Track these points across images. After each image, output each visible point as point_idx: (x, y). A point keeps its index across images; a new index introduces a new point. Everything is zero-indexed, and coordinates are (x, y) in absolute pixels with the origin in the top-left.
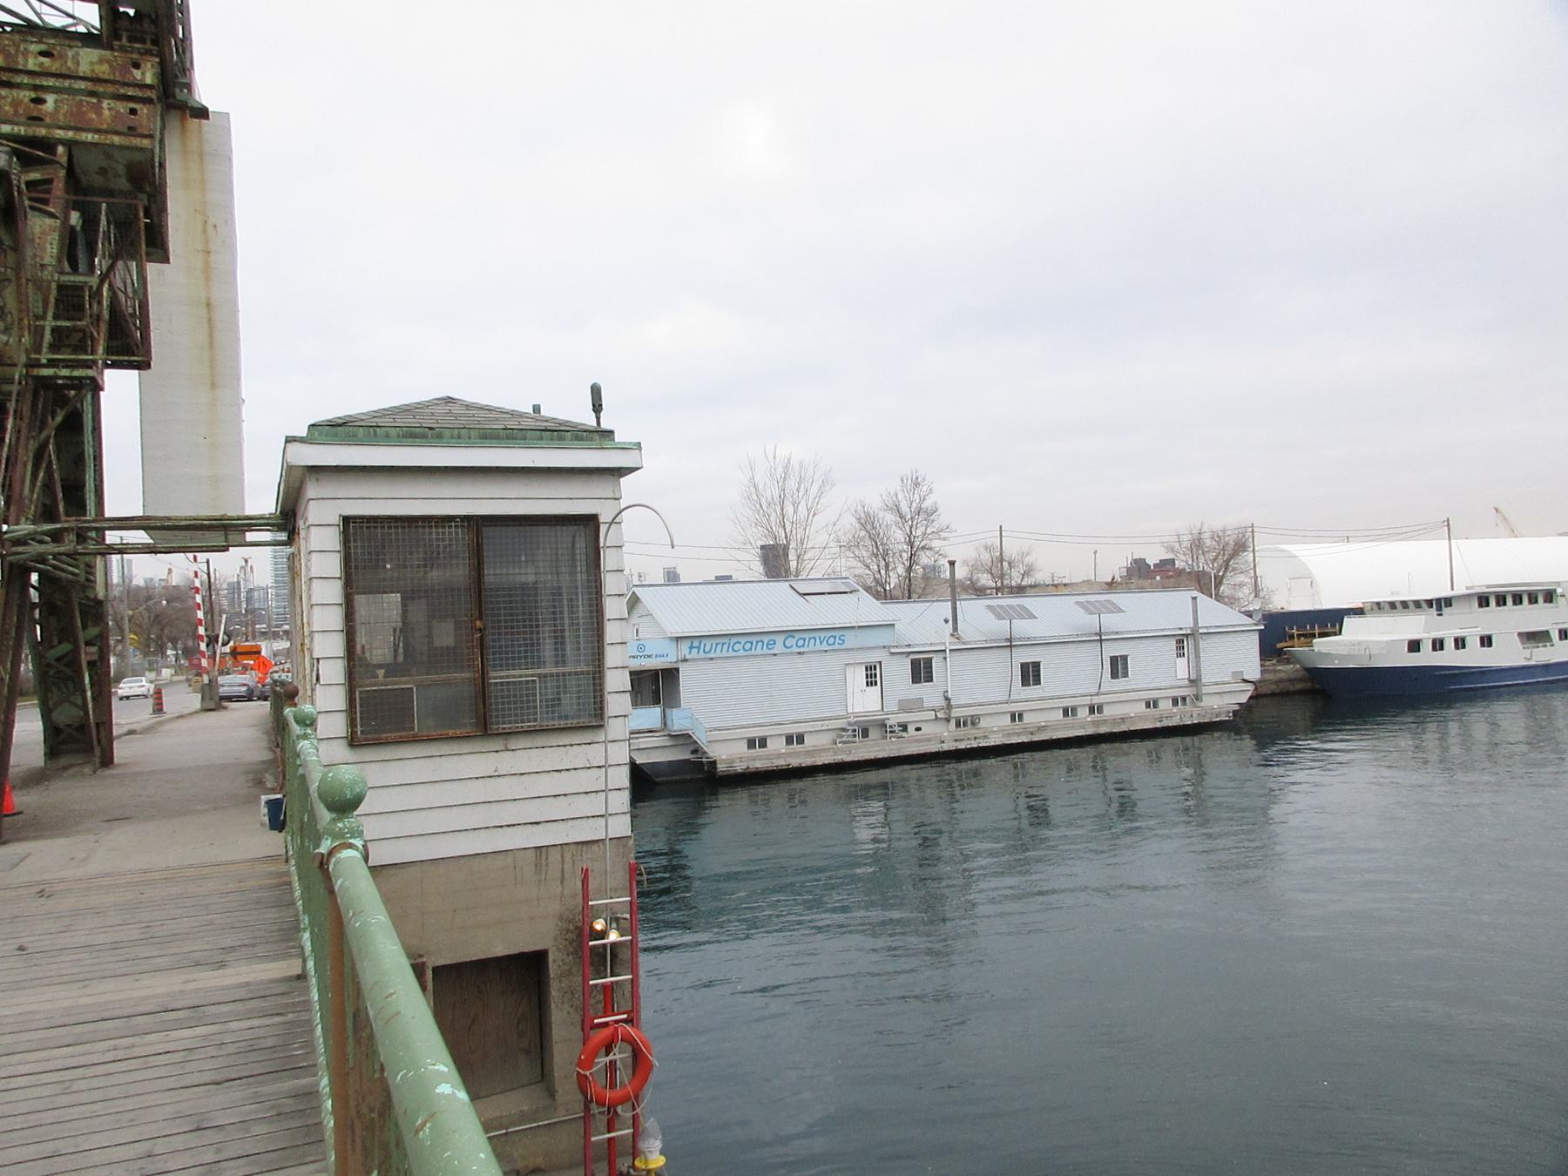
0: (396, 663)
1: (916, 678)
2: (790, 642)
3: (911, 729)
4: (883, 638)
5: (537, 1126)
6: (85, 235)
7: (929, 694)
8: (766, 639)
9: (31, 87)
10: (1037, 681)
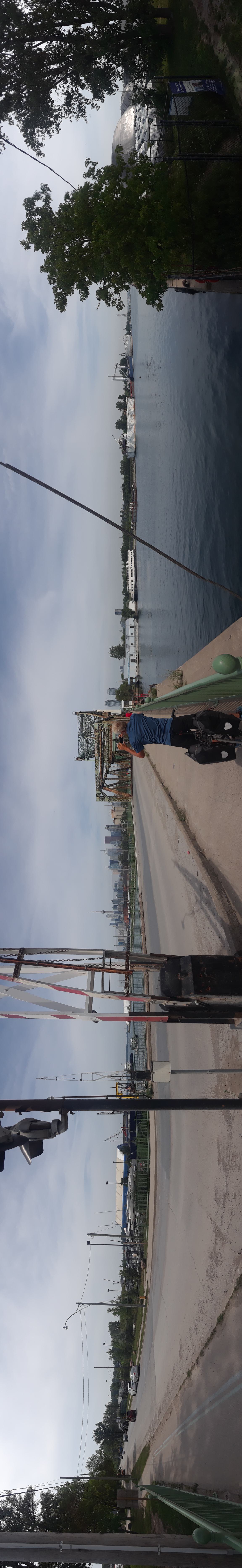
7: (134, 654)
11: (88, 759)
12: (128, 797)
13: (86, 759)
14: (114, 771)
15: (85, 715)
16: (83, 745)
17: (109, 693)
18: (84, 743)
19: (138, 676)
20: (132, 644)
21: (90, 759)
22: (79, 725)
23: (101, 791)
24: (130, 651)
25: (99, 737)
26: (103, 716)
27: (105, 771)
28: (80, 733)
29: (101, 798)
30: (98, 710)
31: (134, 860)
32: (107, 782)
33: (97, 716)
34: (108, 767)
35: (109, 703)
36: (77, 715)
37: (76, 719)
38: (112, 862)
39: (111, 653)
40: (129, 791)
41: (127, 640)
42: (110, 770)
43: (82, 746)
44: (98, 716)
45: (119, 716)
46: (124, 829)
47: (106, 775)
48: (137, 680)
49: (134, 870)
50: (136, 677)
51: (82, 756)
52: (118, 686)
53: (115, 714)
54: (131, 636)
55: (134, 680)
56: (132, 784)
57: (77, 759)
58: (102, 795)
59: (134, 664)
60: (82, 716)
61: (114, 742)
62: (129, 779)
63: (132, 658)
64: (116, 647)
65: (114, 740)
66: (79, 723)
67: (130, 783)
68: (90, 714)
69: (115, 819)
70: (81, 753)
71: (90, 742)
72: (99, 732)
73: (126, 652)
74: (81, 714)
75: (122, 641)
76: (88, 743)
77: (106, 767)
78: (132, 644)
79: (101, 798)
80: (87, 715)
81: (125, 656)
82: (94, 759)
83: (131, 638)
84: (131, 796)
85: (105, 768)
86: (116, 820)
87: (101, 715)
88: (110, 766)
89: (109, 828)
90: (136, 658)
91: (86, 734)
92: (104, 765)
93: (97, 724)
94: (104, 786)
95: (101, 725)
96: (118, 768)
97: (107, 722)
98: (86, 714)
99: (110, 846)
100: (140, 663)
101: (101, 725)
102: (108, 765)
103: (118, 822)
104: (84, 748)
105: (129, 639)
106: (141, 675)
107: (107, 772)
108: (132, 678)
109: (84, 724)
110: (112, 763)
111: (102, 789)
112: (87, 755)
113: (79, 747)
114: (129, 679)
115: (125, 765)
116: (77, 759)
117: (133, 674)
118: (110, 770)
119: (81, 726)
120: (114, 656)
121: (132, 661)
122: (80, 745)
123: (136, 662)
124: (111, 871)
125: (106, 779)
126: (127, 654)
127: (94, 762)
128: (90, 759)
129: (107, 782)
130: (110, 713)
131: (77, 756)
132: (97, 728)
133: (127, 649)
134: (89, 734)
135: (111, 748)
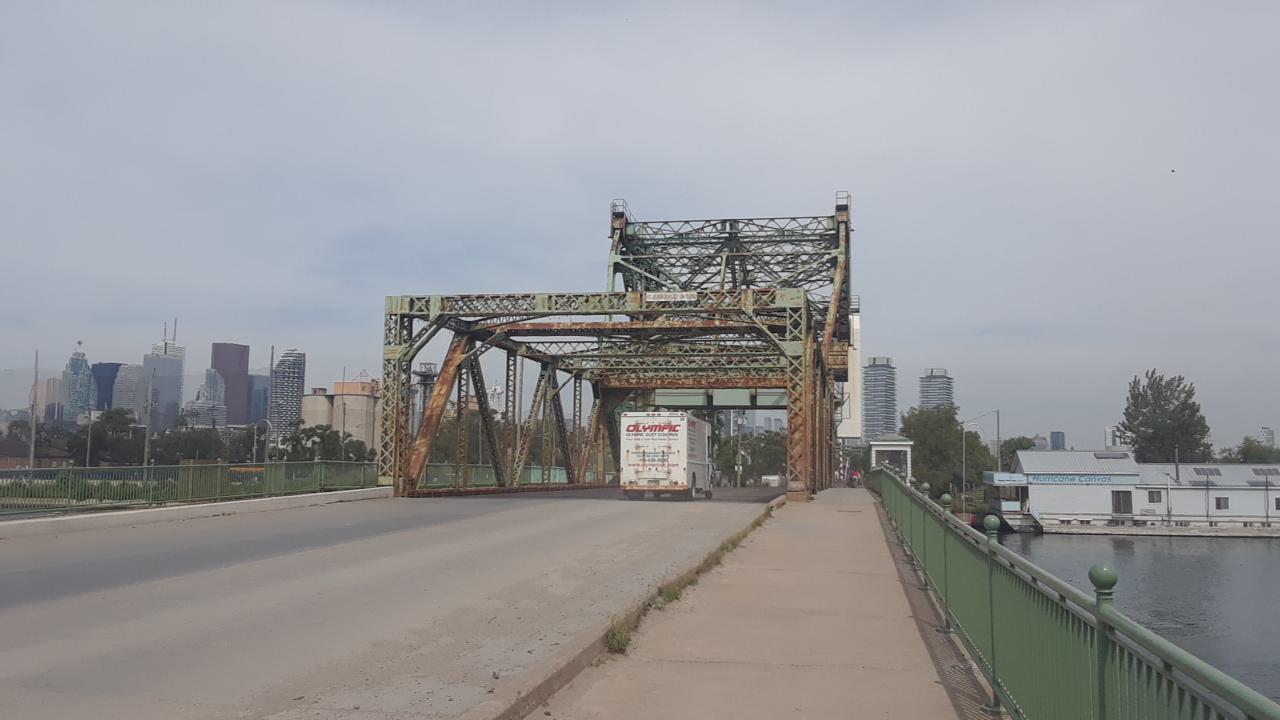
0: (929, 490)
1: (1151, 500)
2: (1082, 479)
3: (1149, 523)
4: (1136, 480)
5: (933, 603)
6: (590, 648)
7: (1160, 509)
8: (1070, 477)
9: (652, 495)
10: (1227, 507)
11: (617, 267)
12: (403, 470)
13: (618, 258)
14: (556, 398)
15: (834, 252)
16: (685, 245)
17: (930, 381)
18: (693, 251)
19: (1038, 531)
20: (1221, 503)
21: (619, 275)
22: (782, 224)
23: (441, 322)
24: (1178, 486)
25: (726, 314)
26: (831, 344)
27: (554, 350)
28: (746, 231)
29: (405, 323)
30: (855, 321)
31: (84, 497)
32: (492, 361)
33: (832, 310)
34: (577, 364)
35: (881, 374)
36: (832, 212)
37: (812, 207)
38: (106, 375)
39: (1155, 383)
40: (447, 476)
41: (1246, 472)
42: (562, 376)
43: (682, 240)
44: (830, 317)
45: (833, 425)
46: (276, 441)
47: (534, 356)
48: (1014, 522)
49: (29, 494)
50: (1029, 516)
51: (633, 237)
52: (969, 419)
53: (839, 404)
54: (1214, 495)
55: (1015, 506)
56: (477, 493)
57: (618, 216)
58: (418, 325)
59: (1106, 507)
60: (834, 240)
61: (700, 401)
62: (507, 478)
63: (1140, 502)
64: (1195, 409)
65: (710, 398)
66: (793, 225)
67: (490, 480)
68: (838, 279)
69: (331, 398)
70: (647, 234)
71: (700, 278)
72: (758, 313)
73: (1170, 468)
74: (836, 234)
75: (1236, 444)
76: (694, 273)
77: (572, 356)
78: (1221, 503)
79: (405, 321)
80: (834, 261)
81: (1141, 458)
82: (620, 287)
83: (1258, 497)
84: (410, 489)
85: (568, 349)
86: (323, 402)
87: (834, 335)
88: (578, 376)
89: (293, 369)
90: (1136, 523)
91: (743, 260)
92: (588, 343)
93: (801, 304)
94: (471, 343)
95: (796, 325)
96: (496, 404)
97: (808, 358)
98: (841, 259)
99: (197, 367)
100: (1107, 546)
101: (796, 325)
102: (586, 365)
103: (315, 413)
104: (674, 251)
105: (1254, 485)
106: (1039, 546)
107: (549, 363)
108: (1021, 493)
109: (788, 248)
110: (595, 387)
111: (458, 333)
112: (637, 262)
113: (676, 227)
114: (1018, 479)
115: (585, 451)
116: (618, 216)
117: (1046, 503)
118: (562, 376)
119: (782, 231)
120: (1137, 398)
121: (1122, 500)
122: (686, 229)
123: (1113, 522)
124: (56, 365)
125: (512, 353)
126: (1157, 473)
127: (604, 290)
128: (619, 275)
129: (492, 361)
130: (842, 376)
131: (635, 214)
132: (778, 304)
133: (1188, 472)
134: (739, 276)
135: (674, 385)
